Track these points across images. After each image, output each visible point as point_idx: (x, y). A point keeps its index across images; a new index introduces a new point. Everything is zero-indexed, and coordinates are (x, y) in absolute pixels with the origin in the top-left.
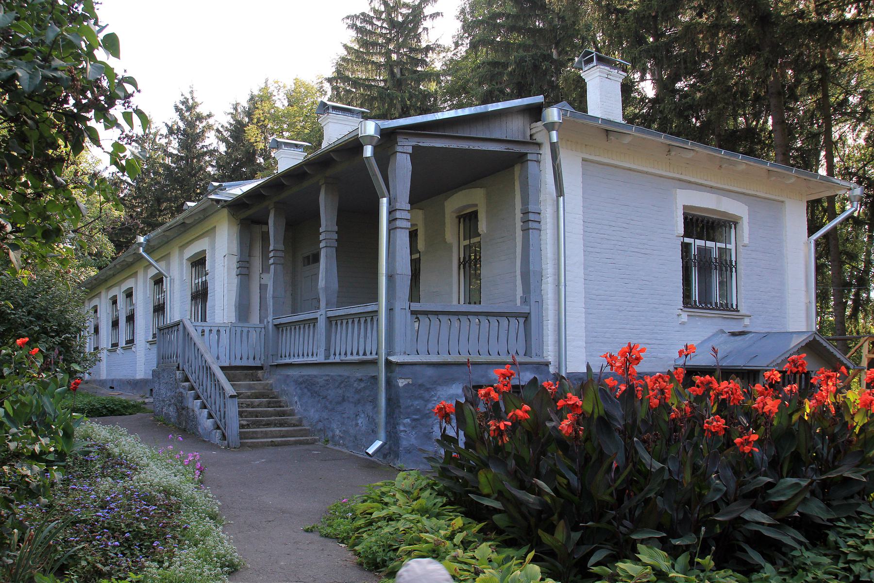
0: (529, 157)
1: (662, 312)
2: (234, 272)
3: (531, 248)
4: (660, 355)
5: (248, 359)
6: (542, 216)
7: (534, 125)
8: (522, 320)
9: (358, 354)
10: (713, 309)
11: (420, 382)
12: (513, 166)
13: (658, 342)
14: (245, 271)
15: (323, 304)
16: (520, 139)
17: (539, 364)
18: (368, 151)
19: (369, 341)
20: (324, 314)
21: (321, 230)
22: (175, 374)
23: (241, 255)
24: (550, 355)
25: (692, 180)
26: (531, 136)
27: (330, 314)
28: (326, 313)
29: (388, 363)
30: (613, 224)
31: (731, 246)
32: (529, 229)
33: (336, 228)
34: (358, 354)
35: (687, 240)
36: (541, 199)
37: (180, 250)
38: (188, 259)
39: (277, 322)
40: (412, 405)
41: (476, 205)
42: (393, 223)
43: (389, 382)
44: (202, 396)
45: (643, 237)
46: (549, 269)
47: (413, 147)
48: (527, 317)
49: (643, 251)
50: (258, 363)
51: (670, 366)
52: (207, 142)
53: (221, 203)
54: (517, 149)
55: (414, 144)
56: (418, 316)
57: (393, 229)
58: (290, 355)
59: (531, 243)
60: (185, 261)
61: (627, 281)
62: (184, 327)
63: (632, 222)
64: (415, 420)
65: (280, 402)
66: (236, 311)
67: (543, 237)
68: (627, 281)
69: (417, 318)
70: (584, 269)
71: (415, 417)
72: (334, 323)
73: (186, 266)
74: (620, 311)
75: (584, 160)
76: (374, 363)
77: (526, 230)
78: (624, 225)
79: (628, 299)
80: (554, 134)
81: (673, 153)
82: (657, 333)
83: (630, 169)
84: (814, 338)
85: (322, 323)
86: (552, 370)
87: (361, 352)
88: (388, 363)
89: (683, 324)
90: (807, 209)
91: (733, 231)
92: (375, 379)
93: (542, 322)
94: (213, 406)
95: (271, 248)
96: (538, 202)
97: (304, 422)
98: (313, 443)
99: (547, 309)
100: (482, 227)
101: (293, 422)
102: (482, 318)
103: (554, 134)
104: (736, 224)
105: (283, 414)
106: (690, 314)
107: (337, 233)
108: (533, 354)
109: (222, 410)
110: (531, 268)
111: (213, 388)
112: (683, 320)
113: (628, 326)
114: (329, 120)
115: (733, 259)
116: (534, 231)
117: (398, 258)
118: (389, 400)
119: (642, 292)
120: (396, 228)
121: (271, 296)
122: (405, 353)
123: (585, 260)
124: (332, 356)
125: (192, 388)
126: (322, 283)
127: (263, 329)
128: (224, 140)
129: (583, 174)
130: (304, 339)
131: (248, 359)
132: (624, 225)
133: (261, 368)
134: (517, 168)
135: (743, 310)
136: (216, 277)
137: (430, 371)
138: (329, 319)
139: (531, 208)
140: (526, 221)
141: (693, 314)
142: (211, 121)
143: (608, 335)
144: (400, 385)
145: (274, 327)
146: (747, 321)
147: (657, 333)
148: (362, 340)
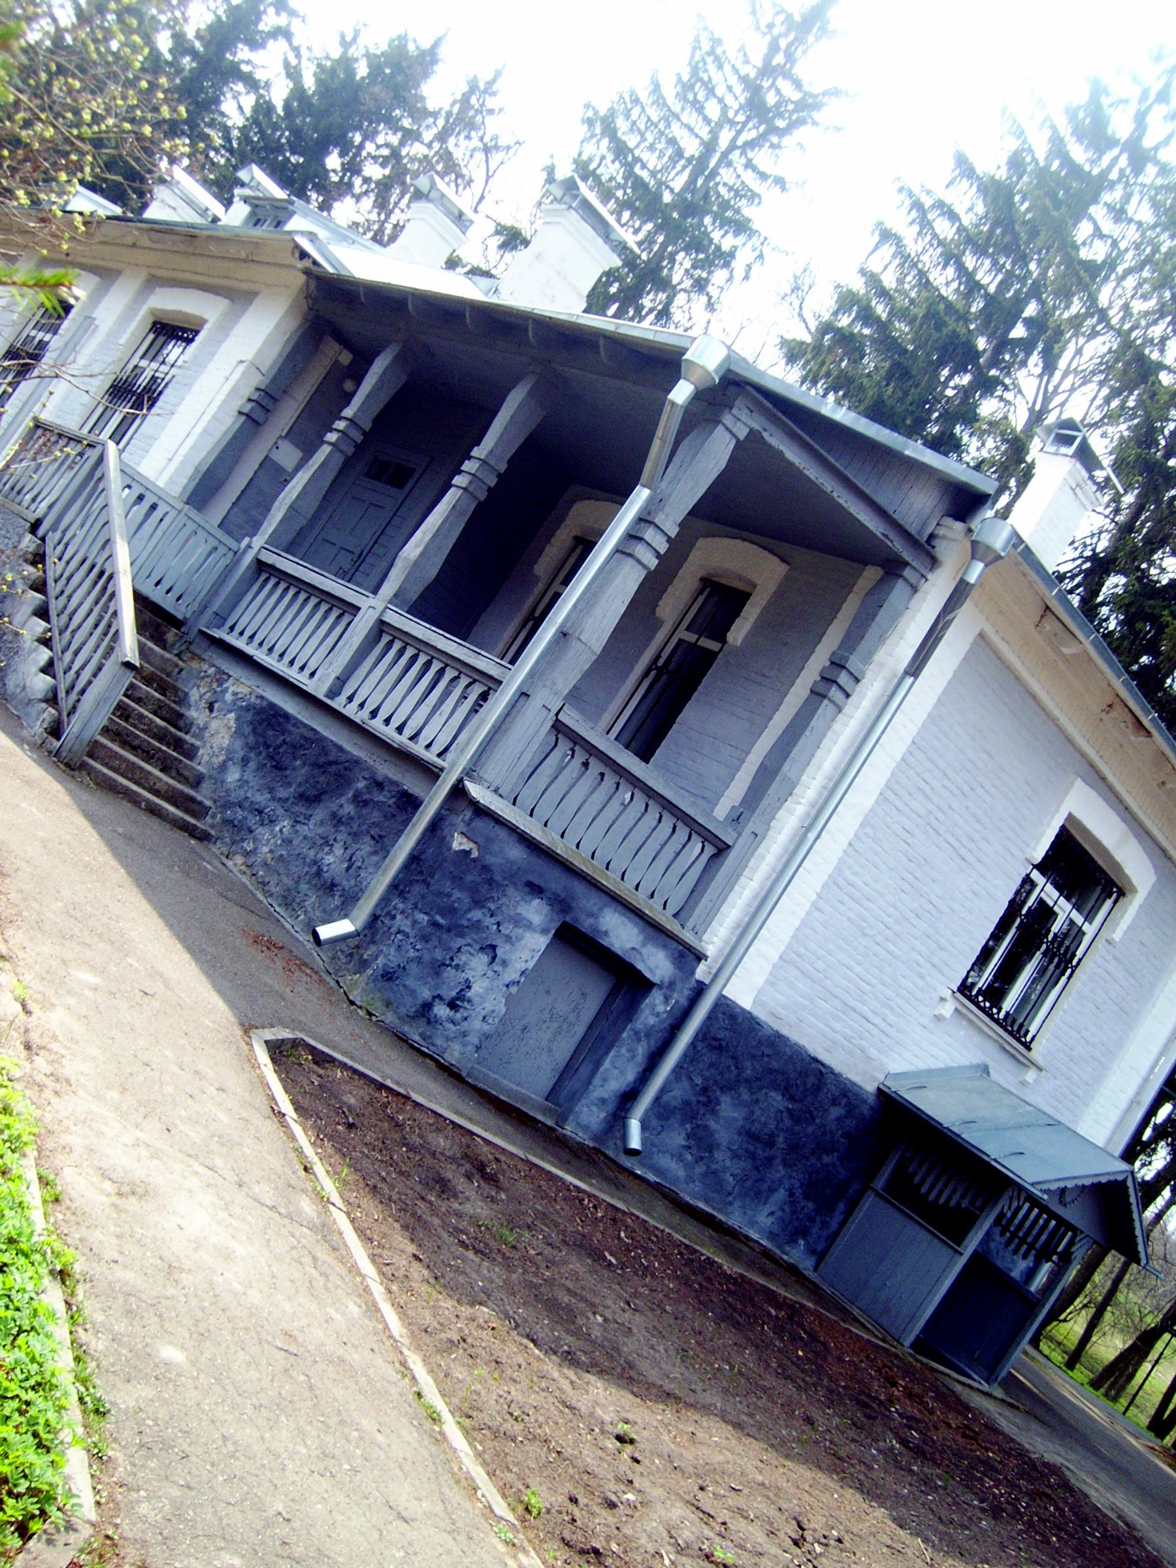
0: (907, 573)
1: (922, 977)
2: (239, 403)
3: (807, 733)
4: (873, 1052)
5: (157, 584)
6: (859, 688)
7: (949, 521)
8: (710, 850)
9: (400, 729)
10: (997, 1021)
11: (490, 860)
12: (865, 563)
13: (883, 1025)
14: (259, 415)
15: (389, 588)
16: (912, 530)
17: (690, 949)
18: (681, 393)
19: (437, 721)
20: (380, 609)
21: (475, 452)
22: (20, 537)
23: (274, 380)
24: (713, 942)
25: (1111, 778)
26: (932, 536)
27: (392, 618)
28: (384, 611)
29: (458, 792)
30: (950, 772)
31: (1089, 929)
32: (824, 696)
33: (502, 467)
34: (400, 729)
35: (1036, 875)
36: (876, 658)
37: (148, 281)
38: (153, 312)
39: (268, 558)
40: (449, 895)
41: (754, 586)
42: (633, 542)
43: (435, 826)
44: (54, 618)
45: (979, 827)
46: (810, 787)
47: (752, 431)
48: (722, 849)
49: (963, 851)
50: (179, 611)
51: (873, 1078)
52: (257, 57)
53: (307, 263)
54: (899, 546)
55: (757, 427)
56: (577, 748)
57: (623, 552)
58: (252, 637)
59: (813, 723)
60: (144, 310)
61: (906, 887)
62: (101, 459)
63: (980, 791)
64: (435, 924)
65: (181, 716)
66: (191, 478)
67: (836, 726)
68: (906, 887)
69: (573, 751)
70: (862, 825)
71: (439, 919)
72: (386, 639)
73: (139, 322)
74: (864, 934)
75: (981, 636)
76: (432, 773)
77: (817, 695)
78: (966, 788)
79: (889, 921)
80: (979, 567)
81: (1114, 714)
82: (892, 1009)
83: (1034, 697)
84: (1125, 1181)
85: (362, 625)
86: (701, 972)
87: (408, 731)
88: (458, 792)
89: (939, 1018)
90: (597, 500)
91: (1108, 903)
92: (410, 804)
93: (739, 876)
94: (68, 656)
95: (348, 412)
96: (868, 659)
97: (206, 786)
98: (200, 839)
99: (763, 858)
100: (738, 633)
101: (186, 773)
102: (639, 796)
103: (979, 567)
104: (1121, 893)
105: (178, 744)
106: (960, 1007)
107: (499, 476)
108: (690, 924)
109: (86, 675)
110: (786, 768)
111: (91, 620)
112: (943, 1012)
113: (858, 969)
114: (562, 220)
115: (1079, 953)
116: (831, 706)
117: (597, 611)
118: (414, 859)
119: (914, 921)
120: (630, 555)
121: (288, 502)
122: (496, 791)
123: (872, 810)
124: (342, 698)
125: (40, 586)
126: (413, 549)
127: (231, 554)
128: (293, 73)
129: (965, 659)
130: (300, 630)
131: (157, 584)
132: (966, 788)
133: (177, 623)
134: (872, 574)
135: (1038, 1051)
136: (195, 388)
137: (516, 853)
138: (382, 627)
139: (853, 663)
140: (827, 680)
141: (964, 1011)
142: (296, 26)
143: (820, 965)
144: (456, 846)
145: (254, 566)
146: (1031, 1075)
147: (892, 1009)
148: (425, 709)
